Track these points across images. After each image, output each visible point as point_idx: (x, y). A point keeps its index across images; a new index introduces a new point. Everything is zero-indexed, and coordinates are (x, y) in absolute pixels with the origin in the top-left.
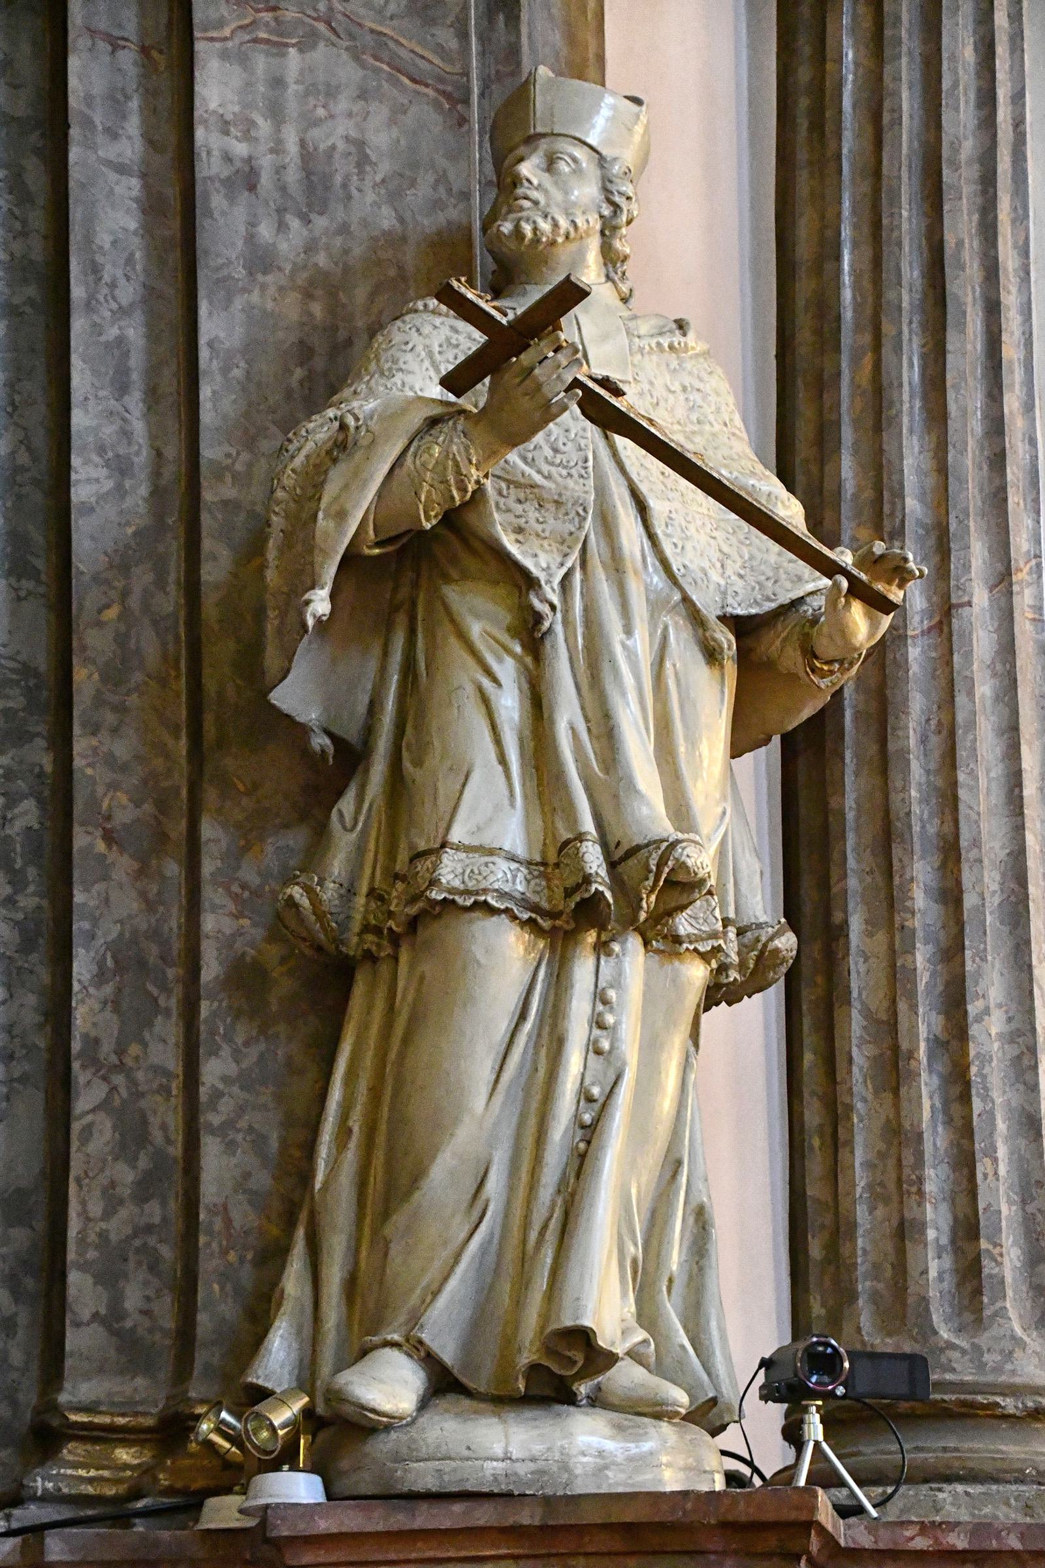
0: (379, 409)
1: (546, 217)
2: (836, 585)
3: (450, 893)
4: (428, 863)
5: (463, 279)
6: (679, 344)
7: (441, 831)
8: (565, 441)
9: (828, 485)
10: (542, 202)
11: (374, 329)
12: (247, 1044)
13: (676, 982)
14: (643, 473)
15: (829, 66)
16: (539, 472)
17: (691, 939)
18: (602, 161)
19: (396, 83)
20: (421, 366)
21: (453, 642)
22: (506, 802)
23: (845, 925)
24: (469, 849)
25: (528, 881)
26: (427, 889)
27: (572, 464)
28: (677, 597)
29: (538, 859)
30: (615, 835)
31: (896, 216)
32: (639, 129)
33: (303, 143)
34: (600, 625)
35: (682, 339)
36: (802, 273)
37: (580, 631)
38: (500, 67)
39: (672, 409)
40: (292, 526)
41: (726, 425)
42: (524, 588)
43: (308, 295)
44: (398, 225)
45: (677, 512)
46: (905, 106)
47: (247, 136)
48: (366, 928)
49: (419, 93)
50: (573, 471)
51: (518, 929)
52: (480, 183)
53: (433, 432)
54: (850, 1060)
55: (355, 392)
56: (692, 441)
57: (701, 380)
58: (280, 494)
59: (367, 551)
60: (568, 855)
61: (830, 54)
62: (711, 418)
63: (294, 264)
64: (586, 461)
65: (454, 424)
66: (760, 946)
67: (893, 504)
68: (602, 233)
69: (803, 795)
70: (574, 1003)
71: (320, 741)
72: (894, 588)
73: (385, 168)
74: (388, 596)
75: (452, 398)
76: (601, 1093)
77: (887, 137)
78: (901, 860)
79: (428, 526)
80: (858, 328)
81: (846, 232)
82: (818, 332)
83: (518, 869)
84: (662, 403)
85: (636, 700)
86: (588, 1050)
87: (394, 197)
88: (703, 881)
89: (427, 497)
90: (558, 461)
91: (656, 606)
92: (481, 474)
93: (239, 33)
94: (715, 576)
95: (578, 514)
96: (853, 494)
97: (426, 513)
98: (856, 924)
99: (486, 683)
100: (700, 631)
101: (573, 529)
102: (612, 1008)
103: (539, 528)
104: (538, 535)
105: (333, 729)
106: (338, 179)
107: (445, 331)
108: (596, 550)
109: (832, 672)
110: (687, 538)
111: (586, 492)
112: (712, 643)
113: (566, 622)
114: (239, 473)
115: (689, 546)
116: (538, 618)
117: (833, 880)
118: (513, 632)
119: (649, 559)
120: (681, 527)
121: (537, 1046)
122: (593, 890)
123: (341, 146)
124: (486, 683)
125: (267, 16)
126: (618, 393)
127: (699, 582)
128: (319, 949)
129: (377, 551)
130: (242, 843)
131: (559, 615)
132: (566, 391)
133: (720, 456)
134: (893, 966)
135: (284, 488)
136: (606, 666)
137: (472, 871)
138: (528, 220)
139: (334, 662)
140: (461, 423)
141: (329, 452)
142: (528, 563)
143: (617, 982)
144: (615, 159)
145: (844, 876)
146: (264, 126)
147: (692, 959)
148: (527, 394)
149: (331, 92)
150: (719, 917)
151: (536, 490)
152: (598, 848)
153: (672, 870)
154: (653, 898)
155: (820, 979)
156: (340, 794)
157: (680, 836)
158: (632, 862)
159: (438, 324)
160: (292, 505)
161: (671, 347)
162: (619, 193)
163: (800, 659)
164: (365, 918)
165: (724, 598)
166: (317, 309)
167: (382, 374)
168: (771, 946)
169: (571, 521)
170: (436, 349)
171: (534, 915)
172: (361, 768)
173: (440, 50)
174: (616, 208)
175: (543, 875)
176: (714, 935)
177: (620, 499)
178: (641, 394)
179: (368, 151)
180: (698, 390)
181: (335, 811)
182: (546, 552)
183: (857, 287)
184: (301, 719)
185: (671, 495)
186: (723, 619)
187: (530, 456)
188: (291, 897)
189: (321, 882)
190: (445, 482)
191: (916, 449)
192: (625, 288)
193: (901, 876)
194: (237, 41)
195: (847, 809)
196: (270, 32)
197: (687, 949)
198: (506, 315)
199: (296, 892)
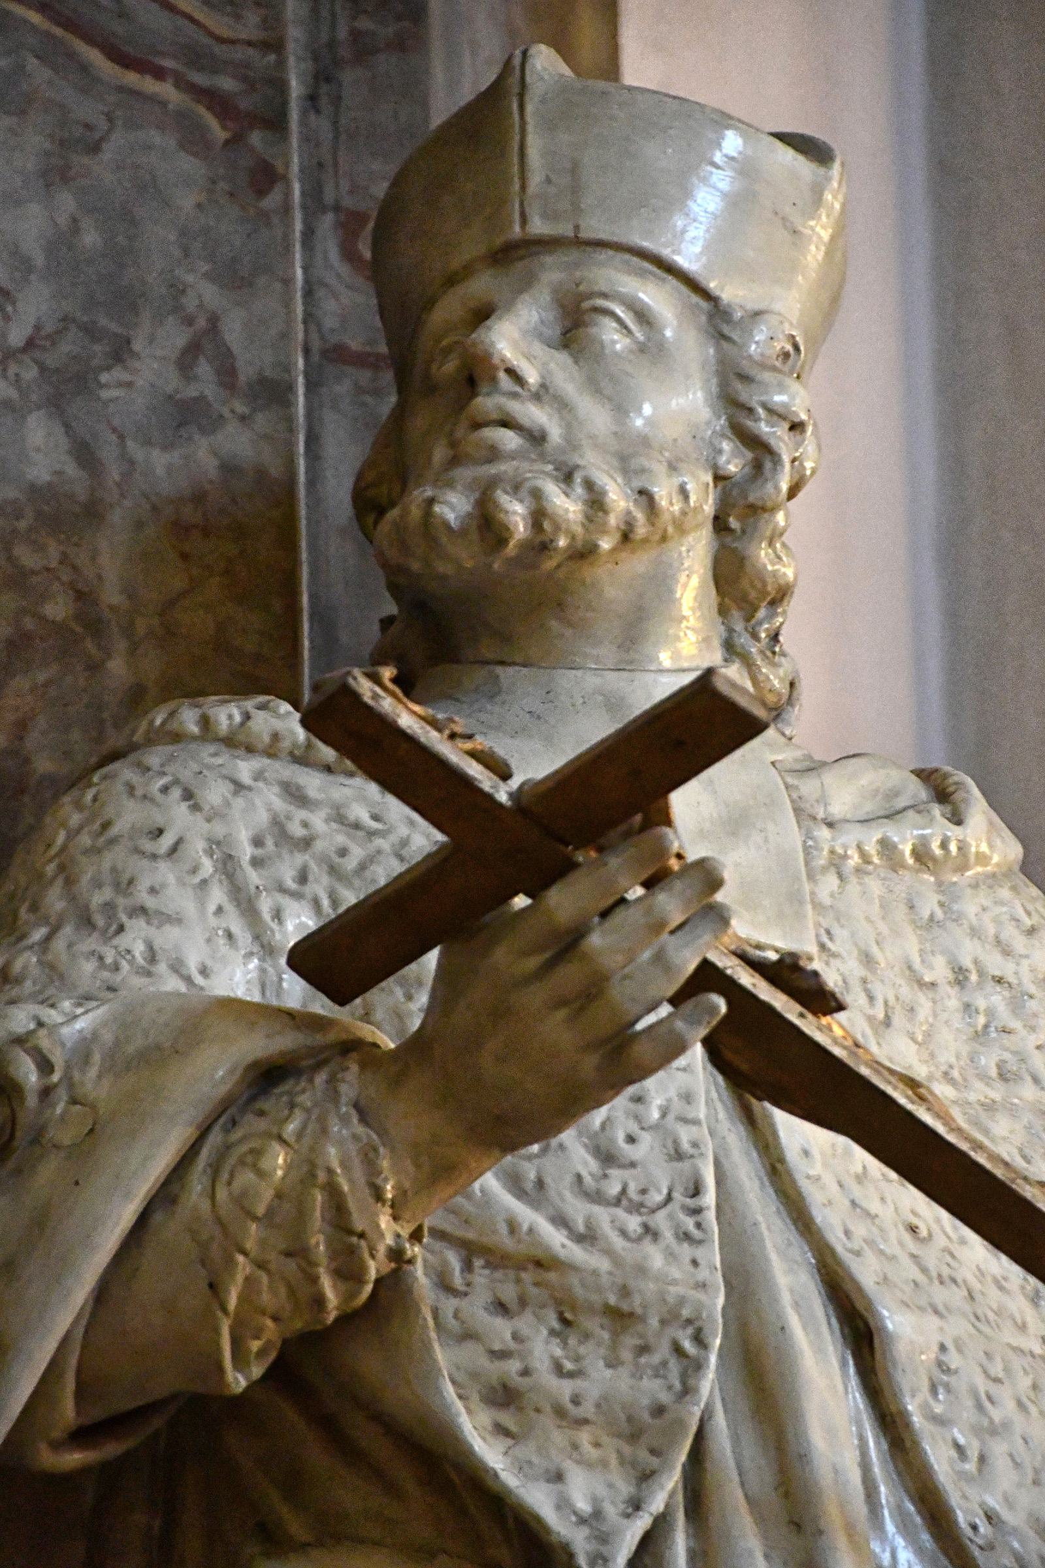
0: (108, 1037)
5: (387, 673)
6: (944, 845)
8: (633, 1127)
10: (555, 433)
14: (860, 1230)
16: (560, 1221)
20: (202, 904)
27: (658, 1197)
32: (821, 229)
35: (954, 832)
38: (364, 24)
44: (71, 469)
50: (660, 1220)
52: (307, 351)
53: (266, 1104)
57: (1007, 952)
64: (696, 1191)
65: (332, 1081)
68: (720, 524)
75: (321, 1006)
79: (237, 1382)
84: (898, 1019)
89: (243, 1299)
90: (614, 1189)
92: (405, 1231)
95: (678, 1350)
97: (236, 1342)
101: (665, 1397)
103: (565, 1389)
104: (560, 1412)
107: (268, 800)
108: (731, 1463)
110: (995, 1430)
111: (702, 1286)
115: (999, 1449)
129: (74, 1459)
132: (675, 1001)
138: (516, 489)
144: (757, 314)
148: (561, 1003)
151: (552, 1276)
159: (245, 777)
161: (921, 855)
162: (770, 411)
167: (86, 922)
169: (659, 1371)
170: (246, 851)
177: (796, 1305)
180: (999, 981)
182: (587, 1464)
185: (940, 1295)
190: (298, 1252)
198: (505, 776)
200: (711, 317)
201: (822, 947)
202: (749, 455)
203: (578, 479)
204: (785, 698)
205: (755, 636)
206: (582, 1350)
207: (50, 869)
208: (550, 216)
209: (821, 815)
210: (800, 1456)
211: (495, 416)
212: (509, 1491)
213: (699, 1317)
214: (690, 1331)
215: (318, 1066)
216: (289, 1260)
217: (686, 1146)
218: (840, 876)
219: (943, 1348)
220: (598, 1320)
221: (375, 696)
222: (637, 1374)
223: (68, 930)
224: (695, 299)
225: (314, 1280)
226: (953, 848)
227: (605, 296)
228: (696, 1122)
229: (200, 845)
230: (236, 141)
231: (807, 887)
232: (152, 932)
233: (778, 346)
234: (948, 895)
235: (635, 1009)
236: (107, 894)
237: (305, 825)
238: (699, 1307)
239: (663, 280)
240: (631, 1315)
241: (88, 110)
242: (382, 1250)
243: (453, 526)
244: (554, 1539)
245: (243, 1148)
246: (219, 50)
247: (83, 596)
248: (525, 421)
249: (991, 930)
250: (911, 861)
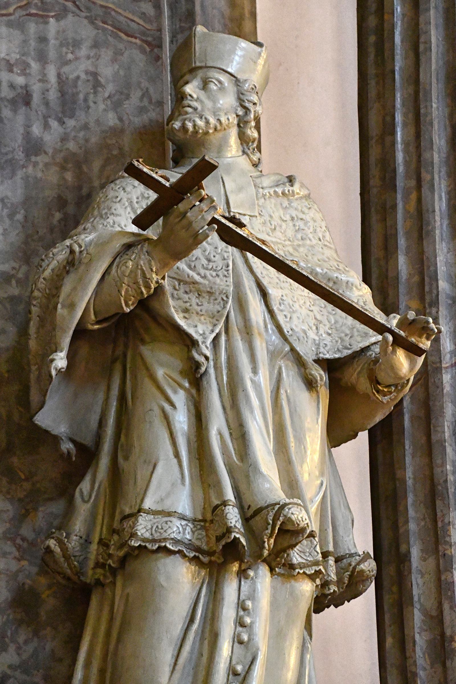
1: (201, 118)
2: (385, 340)
3: (143, 542)
4: (131, 523)
6: (289, 191)
7: (138, 501)
8: (215, 254)
9: (391, 274)
10: (199, 108)
11: (103, 186)
12: (26, 642)
13: (293, 595)
14: (265, 272)
15: (386, 17)
16: (199, 274)
17: (301, 566)
18: (237, 81)
19: (116, 36)
21: (147, 381)
22: (179, 481)
23: (408, 554)
24: (155, 513)
25: (193, 532)
26: (129, 539)
28: (287, 348)
29: (200, 518)
30: (247, 500)
31: (429, 107)
32: (261, 61)
33: (59, 75)
34: (237, 368)
36: (372, 142)
37: (225, 372)
38: (183, 25)
39: (285, 231)
40: (44, 313)
41: (320, 240)
42: (190, 347)
43: (63, 168)
45: (286, 295)
46: (433, 40)
47: (24, 73)
48: (98, 565)
49: (131, 42)
50: (220, 273)
51: (188, 564)
53: (128, 253)
54: (414, 642)
55: (84, 229)
56: (297, 251)
57: (303, 213)
58: (36, 293)
59: (90, 327)
60: (217, 515)
61: (386, 9)
62: (311, 236)
63: (55, 149)
64: (228, 266)
65: (142, 247)
66: (351, 567)
67: (431, 285)
68: (239, 125)
69: (381, 469)
70: (225, 610)
71: (67, 446)
72: (424, 340)
73: (110, 88)
74: (110, 353)
75: (141, 232)
76: (242, 670)
77: (423, 58)
78: (442, 511)
80: (407, 176)
81: (399, 118)
82: (383, 179)
83: (187, 525)
84: (277, 228)
85: (260, 415)
86: (234, 641)
87: (117, 106)
88: (304, 529)
90: (210, 267)
91: (273, 355)
92: (159, 278)
93: (19, 10)
94: (312, 335)
95: (223, 299)
96: (406, 280)
98: (415, 552)
99: (167, 407)
100: (303, 370)
101: (220, 309)
102: (249, 613)
103: (199, 308)
104: (197, 313)
105: (78, 439)
106: (81, 96)
109: (391, 393)
110: (294, 312)
111: (228, 286)
112: (310, 377)
113: (216, 367)
114: (20, 279)
115: (295, 316)
116: (198, 365)
117: (400, 525)
118: (183, 373)
119: (269, 326)
120: (289, 304)
121: (202, 639)
122: (233, 537)
123: (83, 76)
124: (167, 407)
126: (241, 225)
127: (302, 339)
128: (69, 579)
129: (96, 327)
130: (23, 511)
131: (212, 363)
132: (208, 225)
133: (316, 259)
134: (439, 580)
135: (38, 290)
136: (241, 395)
137: (157, 527)
138: (190, 121)
139: (76, 395)
141: (65, 267)
142: (191, 331)
143: (252, 596)
144: (246, 80)
145: (407, 522)
146: (35, 66)
147: (303, 579)
148: (183, 228)
149: (76, 44)
150: (319, 552)
151: (196, 285)
152: (236, 510)
153: (283, 522)
154: (272, 541)
155: (395, 589)
156: (82, 477)
157: (288, 501)
158: (258, 518)
160: (44, 300)
161: (283, 193)
162: (248, 101)
163: (368, 385)
164: (97, 558)
165: (318, 348)
166: (69, 176)
167: (101, 217)
168: (358, 568)
170: (135, 200)
171: (197, 554)
172: (94, 462)
173: (143, 15)
174: (247, 110)
175: (203, 528)
176: (316, 563)
178: (264, 223)
179: (99, 78)
180: (302, 219)
181: (78, 490)
182: (203, 324)
183: (406, 151)
184: (55, 432)
186: (318, 361)
187: (193, 264)
188: (48, 547)
189: (68, 536)
190: (136, 283)
191: (445, 250)
192: (255, 158)
193: (442, 521)
194: (17, 15)
195: (408, 479)
196: (38, 9)
197: (299, 573)
198: (168, 181)
199: (52, 543)
200: (236, 81)
201: (260, 214)
202: (244, 110)
203: (203, 117)
204: (257, 162)
205: (249, 149)
207: (96, 206)
208: (200, 62)
209: (261, 186)
211: (187, 105)
214: (225, 295)
215: (138, 245)
217: (226, 257)
218: (265, 199)
219: (282, 296)
220: (206, 294)
221: (138, 165)
222: (214, 304)
223: (97, 219)
224: (232, 78)
225: (140, 288)
226: (291, 192)
228: (228, 252)
229: (125, 199)
230: (152, 50)
231: (256, 202)
232: (115, 218)
233: (251, 87)
234: (290, 202)
235: (198, 228)
236: (106, 211)
237: (148, 194)
238: (227, 290)
240: (213, 293)
241: (121, 46)
242: (154, 282)
245: (122, 263)
246: (148, 32)
247: (120, 149)
249: (300, 208)
250: (281, 195)
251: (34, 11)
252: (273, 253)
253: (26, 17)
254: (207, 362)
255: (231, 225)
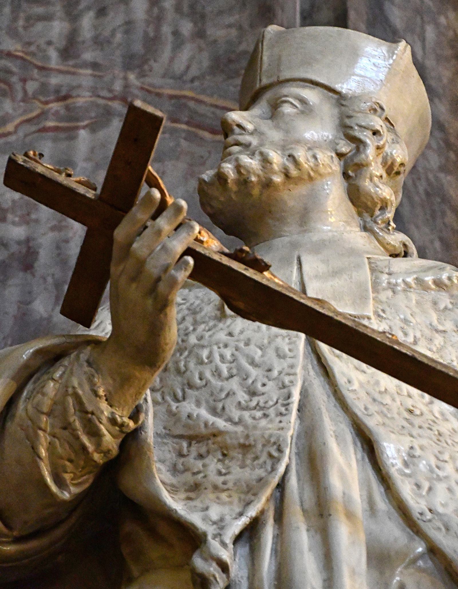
8: (265, 380)
16: (229, 420)
27: (271, 403)
68: (345, 175)
90: (253, 404)
95: (270, 456)
125: (55, 106)
140: (86, 353)
151: (219, 439)
162: (360, 126)
187: (220, 405)
190: (67, 426)
194: (21, 133)
196: (60, 119)
200: (338, 100)
202: (354, 145)
205: (376, 222)
206: (230, 464)
209: (387, 270)
210: (325, 488)
211: (232, 143)
212: (182, 516)
213: (278, 440)
214: (275, 447)
216: (64, 431)
217: (287, 382)
218: (394, 292)
224: (331, 94)
225: (77, 438)
227: (286, 96)
239: (314, 88)
240: (250, 446)
242: (104, 420)
243: (207, 181)
244: (200, 531)
248: (243, 142)
250: (433, 287)
251: (51, 124)
252: (330, 314)
253: (37, 134)
254: (224, 576)
255: (236, 266)
